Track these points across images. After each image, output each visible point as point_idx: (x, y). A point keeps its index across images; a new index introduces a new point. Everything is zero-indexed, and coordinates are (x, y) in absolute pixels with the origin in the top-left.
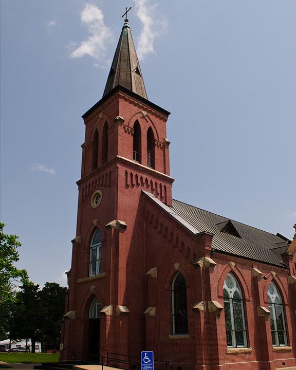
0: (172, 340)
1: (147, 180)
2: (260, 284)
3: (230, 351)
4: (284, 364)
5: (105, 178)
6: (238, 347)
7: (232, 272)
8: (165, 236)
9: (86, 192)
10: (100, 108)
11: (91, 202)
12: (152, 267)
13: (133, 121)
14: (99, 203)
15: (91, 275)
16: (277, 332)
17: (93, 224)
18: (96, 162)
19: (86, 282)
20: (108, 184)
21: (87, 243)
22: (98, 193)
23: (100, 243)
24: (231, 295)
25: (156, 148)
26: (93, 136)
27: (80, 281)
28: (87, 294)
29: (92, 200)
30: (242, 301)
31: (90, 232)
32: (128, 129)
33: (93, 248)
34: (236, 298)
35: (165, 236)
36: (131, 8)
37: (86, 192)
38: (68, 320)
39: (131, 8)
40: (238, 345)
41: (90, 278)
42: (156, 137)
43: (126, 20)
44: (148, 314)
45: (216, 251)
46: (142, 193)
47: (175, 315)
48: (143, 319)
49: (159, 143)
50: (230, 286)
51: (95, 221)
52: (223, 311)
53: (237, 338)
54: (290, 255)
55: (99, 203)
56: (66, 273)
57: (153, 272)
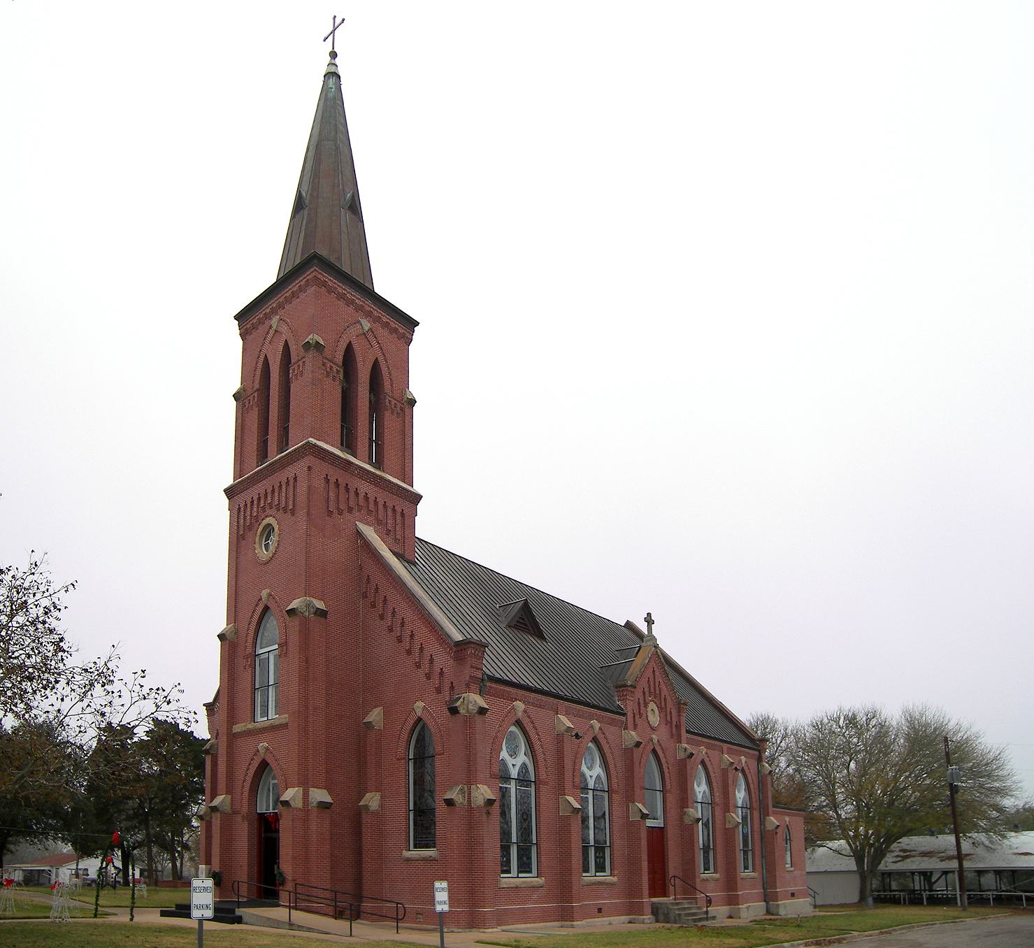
0: (408, 860)
1: (366, 498)
2: (569, 745)
3: (506, 883)
4: (600, 910)
5: (284, 490)
6: (597, 874)
7: (518, 723)
8: (400, 640)
9: (245, 518)
10: (273, 303)
11: (257, 546)
12: (375, 707)
13: (342, 346)
14: (272, 548)
15: (259, 719)
16: (593, 848)
17: (260, 599)
18: (266, 442)
19: (249, 733)
20: (291, 507)
21: (249, 644)
22: (269, 525)
23: (276, 647)
24: (514, 773)
25: (387, 414)
26: (259, 372)
27: (237, 728)
28: (252, 760)
29: (257, 539)
30: (533, 784)
31: (256, 617)
32: (331, 368)
33: (262, 657)
34: (523, 780)
35: (400, 640)
36: (343, 20)
37: (245, 518)
38: (218, 815)
39: (343, 20)
40: (522, 872)
41: (258, 725)
42: (387, 384)
43: (334, 55)
44: (366, 807)
45: (492, 679)
46: (359, 534)
47: (415, 810)
48: (357, 816)
49: (393, 402)
50: (513, 754)
51: (265, 593)
52: (497, 804)
53: (519, 858)
54: (631, 686)
55: (272, 548)
56: (204, 705)
57: (375, 716)
